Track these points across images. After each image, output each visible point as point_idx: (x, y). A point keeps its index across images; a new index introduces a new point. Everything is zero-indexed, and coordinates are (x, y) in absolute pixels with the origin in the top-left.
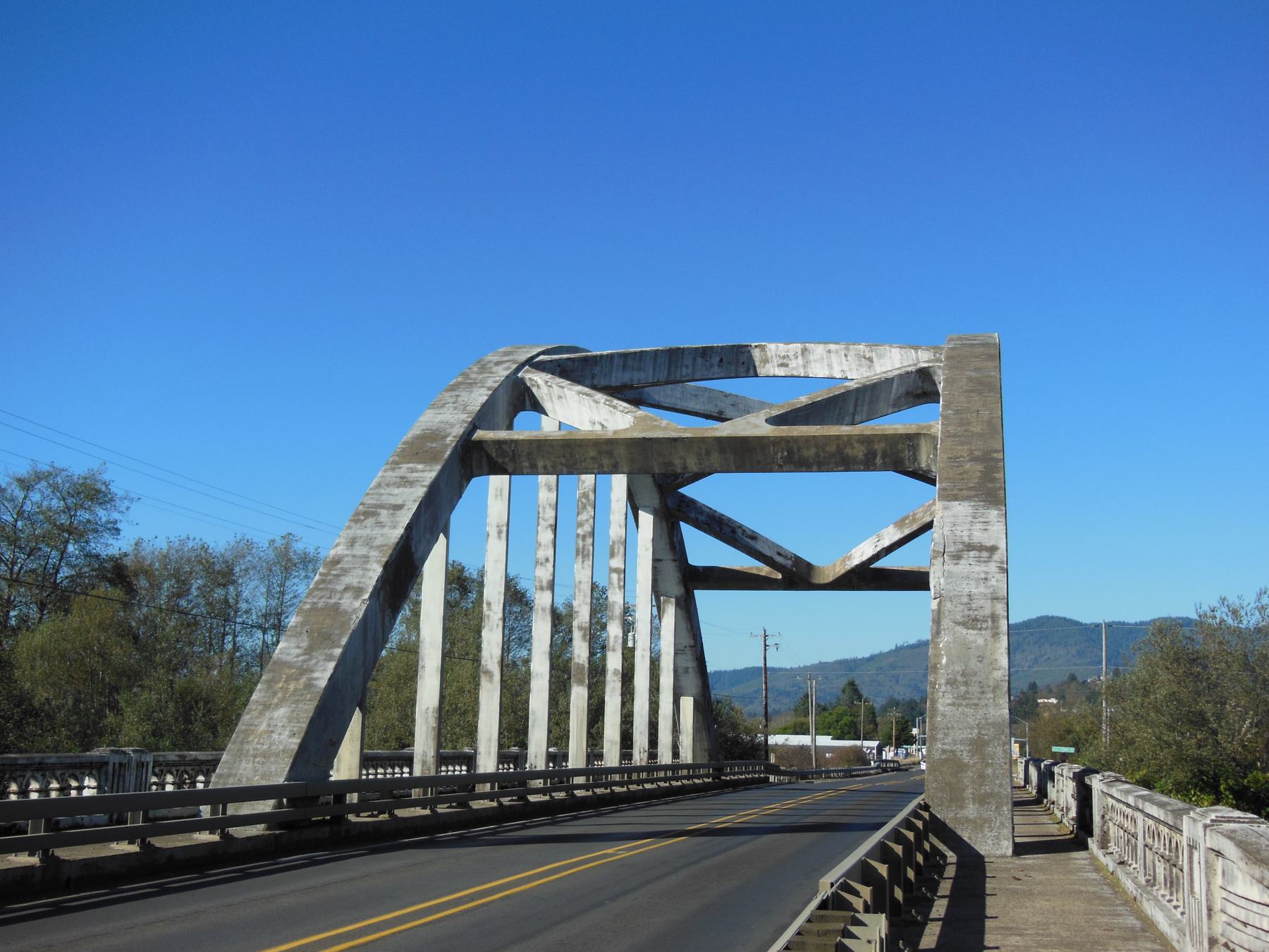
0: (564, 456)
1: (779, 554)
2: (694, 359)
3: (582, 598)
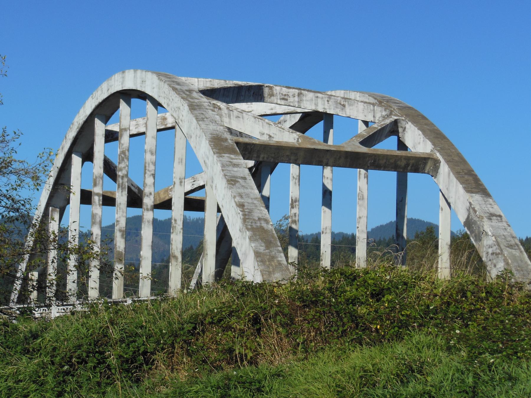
0: (274, 153)
1: (132, 185)
3: (121, 213)
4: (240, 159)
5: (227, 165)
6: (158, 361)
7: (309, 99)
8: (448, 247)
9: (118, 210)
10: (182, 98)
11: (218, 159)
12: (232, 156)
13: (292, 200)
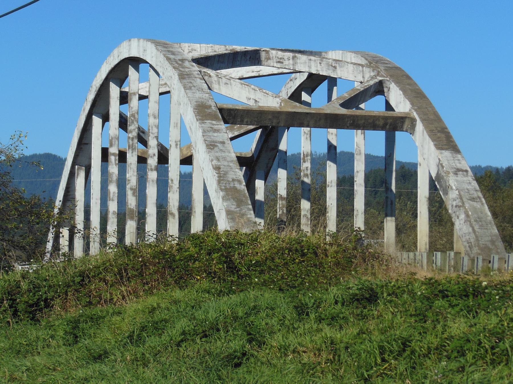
0: (257, 118)
2: (241, 57)
3: (132, 172)
4: (221, 125)
5: (208, 131)
6: (56, 306)
7: (303, 61)
8: (427, 199)
9: (129, 170)
10: (174, 68)
11: (200, 125)
12: (214, 122)
13: (304, 154)
